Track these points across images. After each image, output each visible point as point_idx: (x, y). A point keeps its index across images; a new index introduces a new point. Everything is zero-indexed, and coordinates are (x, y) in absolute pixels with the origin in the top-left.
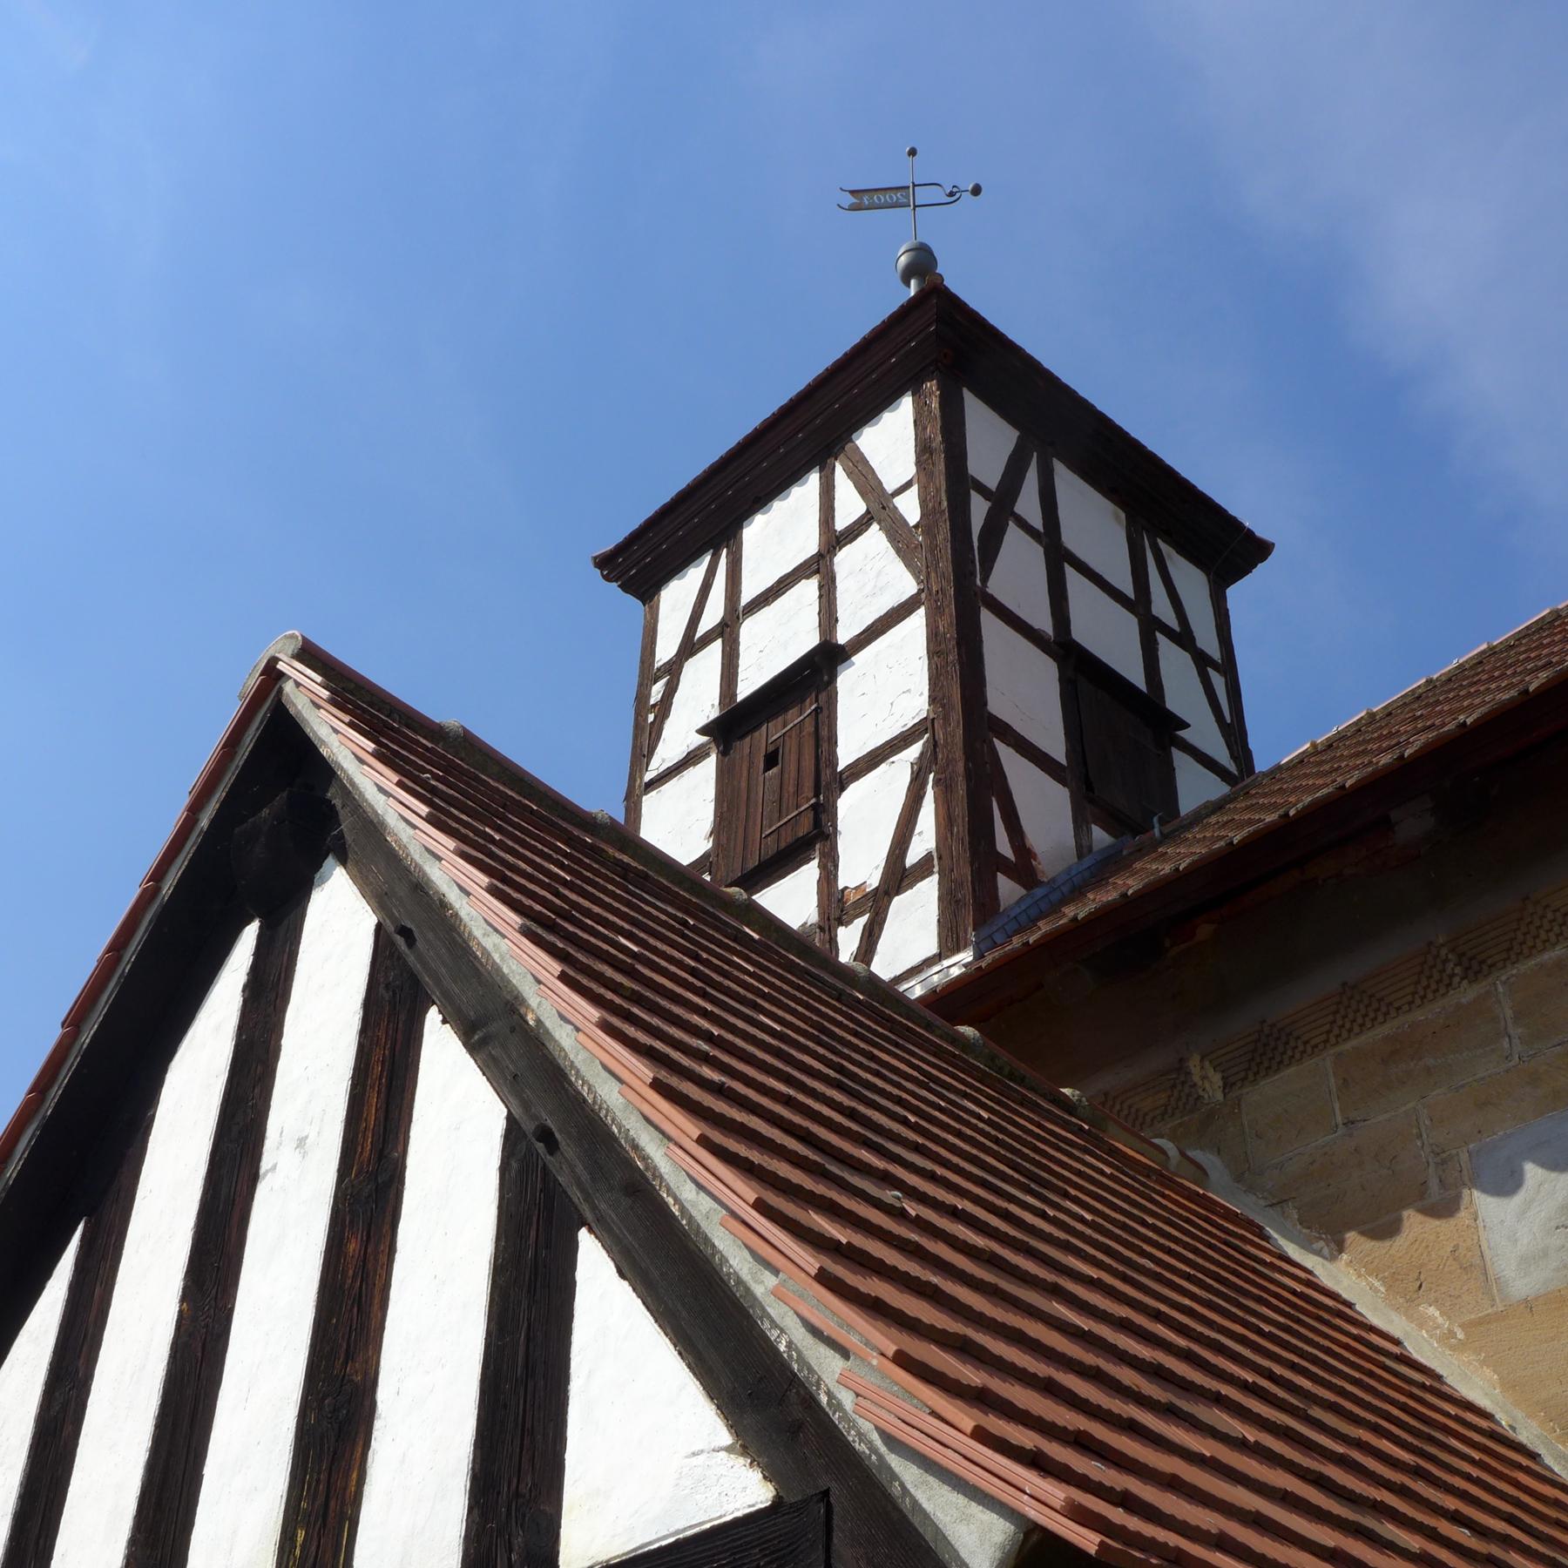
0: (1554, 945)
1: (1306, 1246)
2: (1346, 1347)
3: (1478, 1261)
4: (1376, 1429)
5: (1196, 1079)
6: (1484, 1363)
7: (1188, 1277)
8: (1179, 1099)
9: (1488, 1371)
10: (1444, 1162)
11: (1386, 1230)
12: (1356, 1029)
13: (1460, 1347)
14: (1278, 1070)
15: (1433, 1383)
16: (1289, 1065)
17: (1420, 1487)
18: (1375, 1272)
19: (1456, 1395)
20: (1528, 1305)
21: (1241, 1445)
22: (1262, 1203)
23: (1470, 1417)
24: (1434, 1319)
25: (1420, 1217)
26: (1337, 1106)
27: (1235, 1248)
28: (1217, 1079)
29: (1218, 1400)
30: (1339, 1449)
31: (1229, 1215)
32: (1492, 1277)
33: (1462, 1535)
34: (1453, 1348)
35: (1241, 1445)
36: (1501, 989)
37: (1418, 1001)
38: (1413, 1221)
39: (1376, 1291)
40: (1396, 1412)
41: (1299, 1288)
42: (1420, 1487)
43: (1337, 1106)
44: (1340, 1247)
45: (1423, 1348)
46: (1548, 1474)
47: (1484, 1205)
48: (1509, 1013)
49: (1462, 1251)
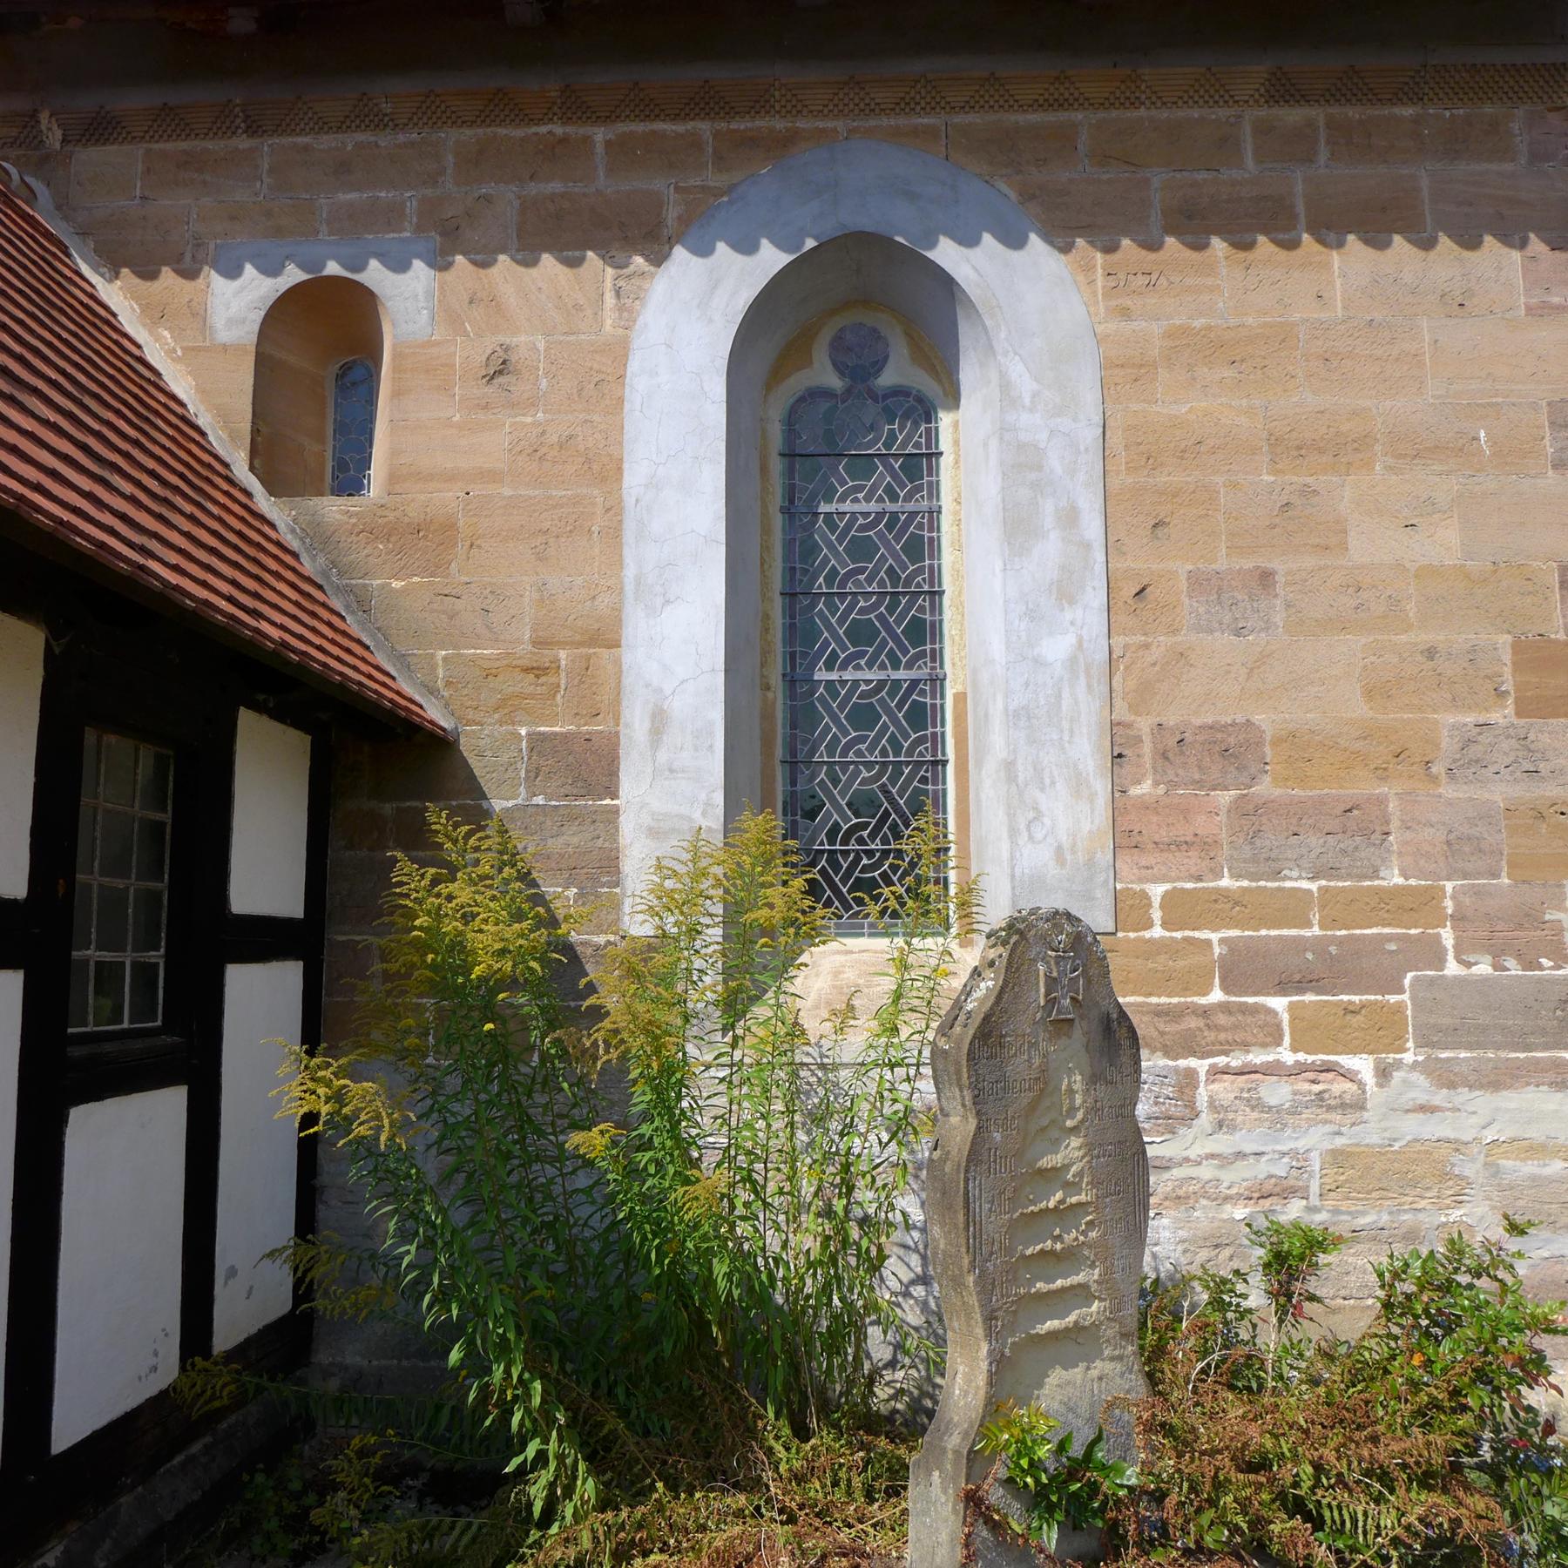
0: (306, 134)
1: (95, 269)
2: (108, 349)
3: (202, 312)
4: (118, 413)
5: (43, 128)
6: (189, 373)
7: (20, 292)
8: (27, 137)
9: (189, 378)
10: (198, 245)
11: (150, 275)
12: (165, 137)
13: (177, 360)
14: (104, 144)
15: (154, 379)
16: (113, 144)
17: (136, 453)
18: (136, 299)
19: (167, 389)
20: (225, 348)
21: (46, 423)
22: (72, 230)
23: (172, 405)
24: (166, 338)
25: (173, 274)
26: (139, 185)
27: (49, 264)
28: (59, 134)
29: (35, 391)
30: (96, 426)
31: (48, 235)
32: (208, 324)
33: (153, 485)
34: (173, 359)
35: (46, 423)
36: (266, 149)
37: (211, 135)
38: (168, 276)
39: (134, 310)
40: (131, 400)
41: (86, 300)
42: (136, 453)
43: (139, 185)
44: (117, 276)
45: (154, 355)
46: (208, 446)
47: (217, 282)
48: (266, 166)
49: (194, 304)
